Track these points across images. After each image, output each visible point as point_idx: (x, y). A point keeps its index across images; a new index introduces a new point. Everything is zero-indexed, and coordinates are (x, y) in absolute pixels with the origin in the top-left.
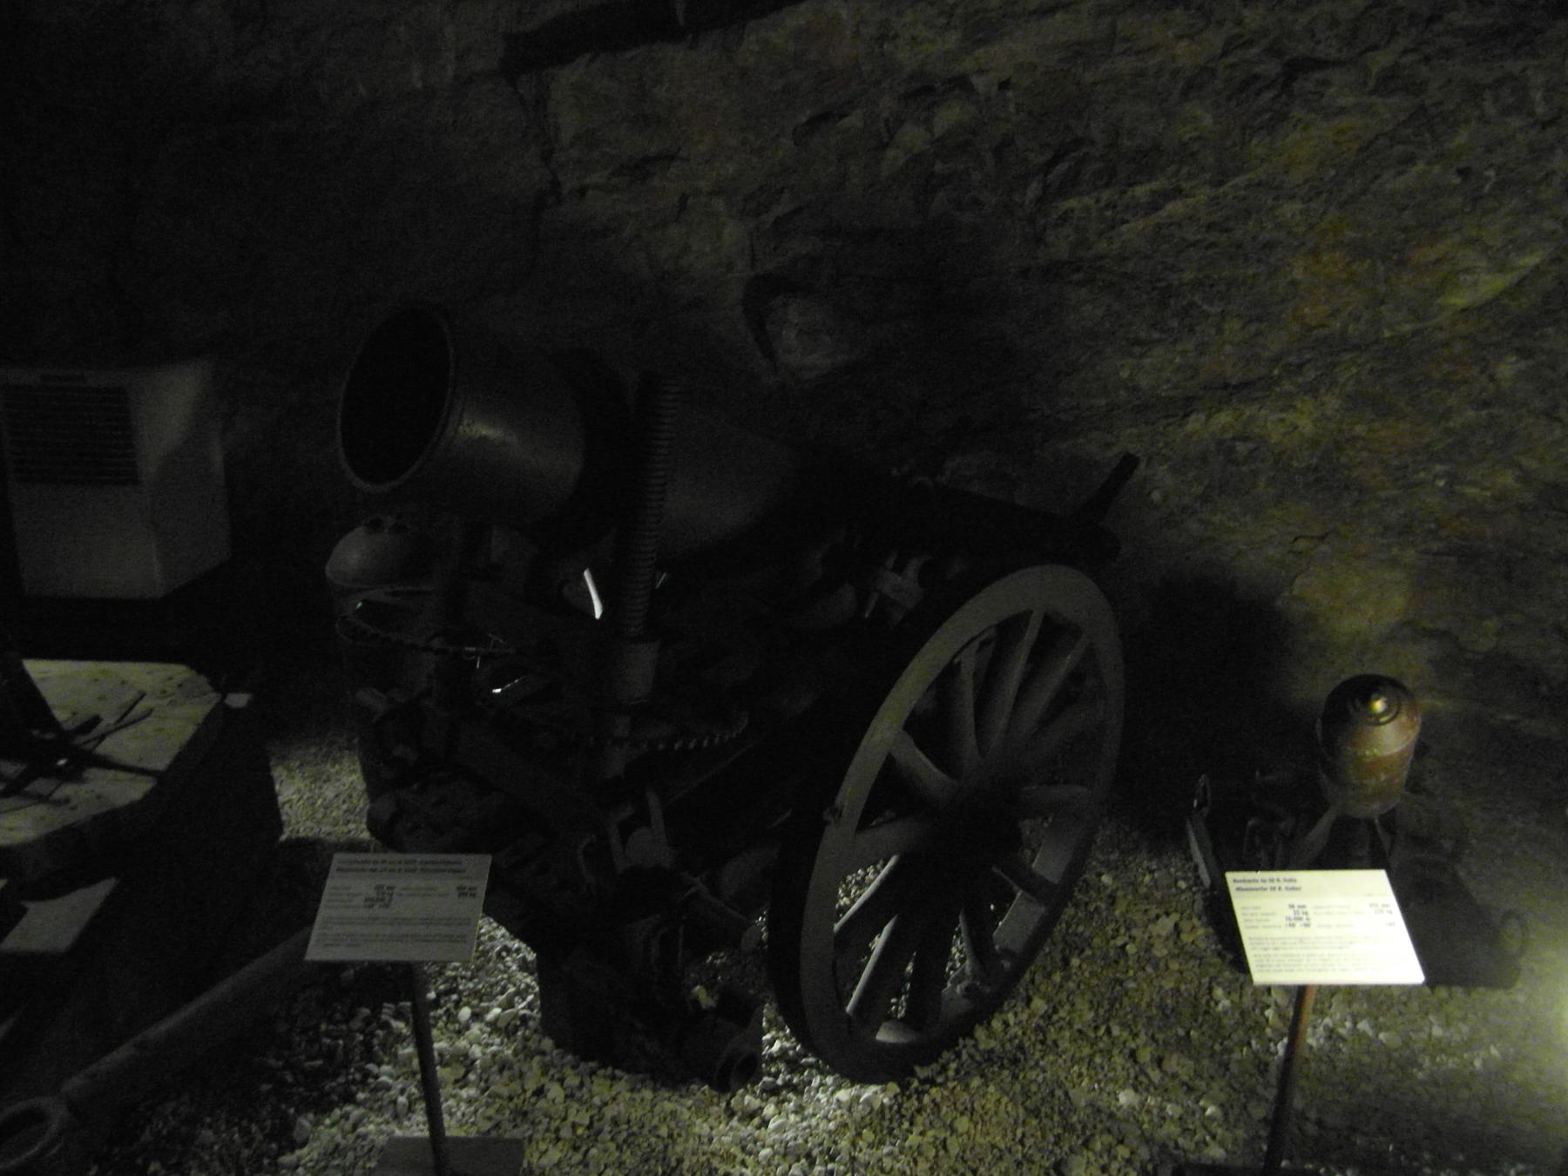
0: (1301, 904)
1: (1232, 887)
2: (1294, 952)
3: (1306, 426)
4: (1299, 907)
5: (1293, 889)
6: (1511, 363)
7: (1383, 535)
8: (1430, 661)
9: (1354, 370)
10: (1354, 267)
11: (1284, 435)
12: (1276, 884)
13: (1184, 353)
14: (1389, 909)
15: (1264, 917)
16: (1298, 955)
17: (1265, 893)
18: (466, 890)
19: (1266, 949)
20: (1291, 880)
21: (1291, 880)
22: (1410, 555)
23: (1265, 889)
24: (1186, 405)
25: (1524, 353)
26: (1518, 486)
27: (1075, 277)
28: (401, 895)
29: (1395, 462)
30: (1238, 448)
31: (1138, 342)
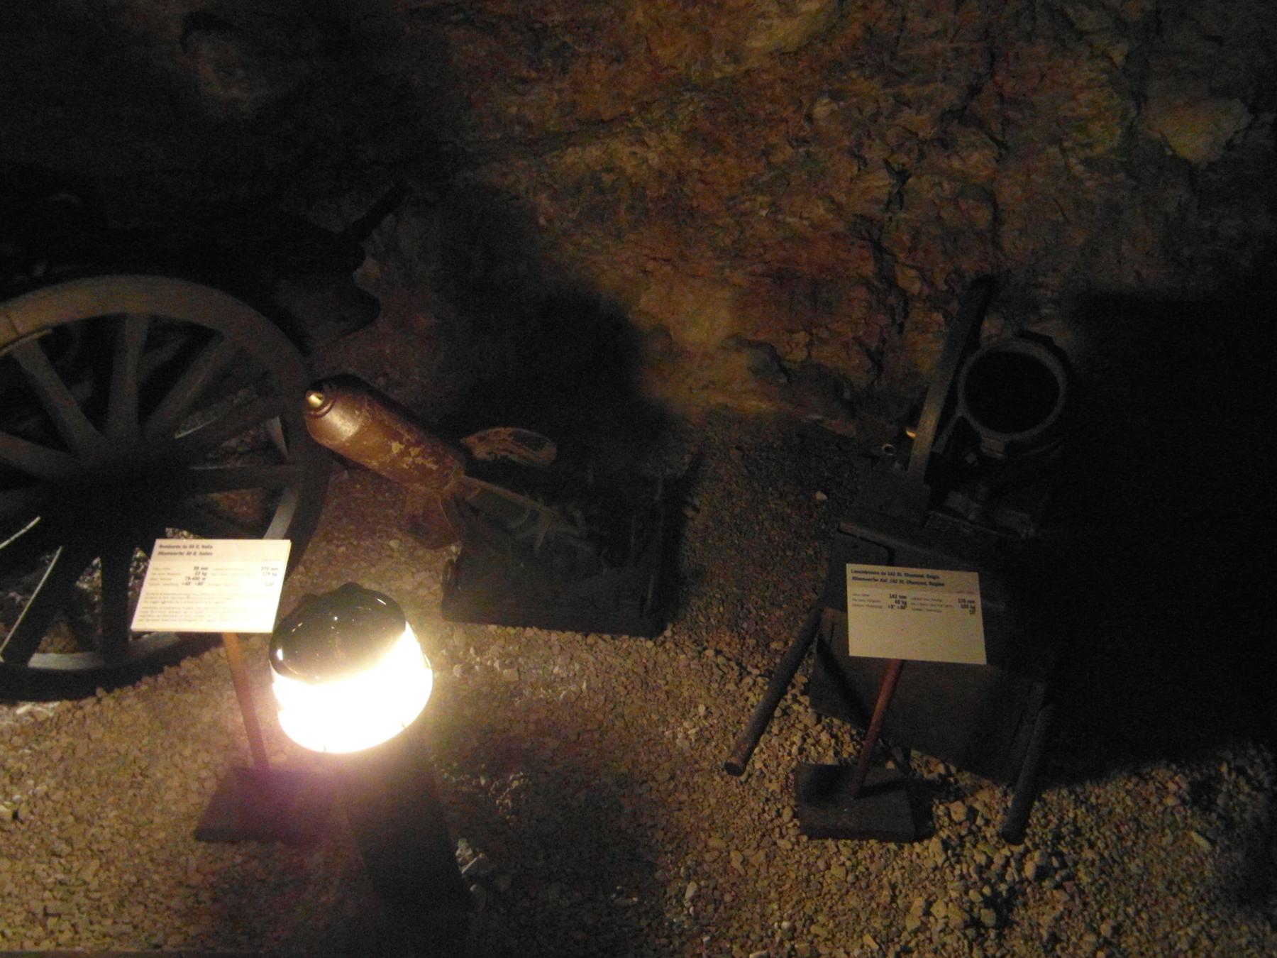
0: (205, 566)
1: (849, 575)
2: (174, 605)
3: (654, 158)
4: (900, 597)
5: (207, 554)
6: (825, 105)
7: (719, 258)
8: (755, 371)
9: (691, 109)
10: (689, 10)
11: (636, 166)
12: (193, 550)
13: (560, 91)
14: (973, 605)
15: (168, 577)
16: (179, 608)
17: (182, 556)
18: (200, 570)
19: (154, 603)
20: (207, 547)
21: (207, 547)
22: (738, 277)
23: (876, 580)
24: (567, 139)
25: (835, 96)
26: (831, 216)
27: (455, 18)
28: (213, 574)
29: (727, 194)
30: (604, 179)
31: (524, 81)
